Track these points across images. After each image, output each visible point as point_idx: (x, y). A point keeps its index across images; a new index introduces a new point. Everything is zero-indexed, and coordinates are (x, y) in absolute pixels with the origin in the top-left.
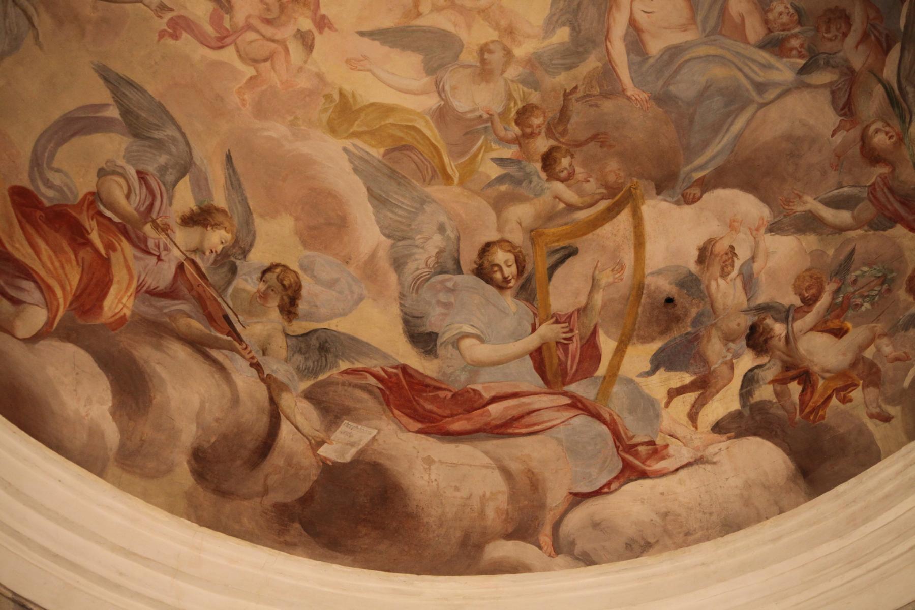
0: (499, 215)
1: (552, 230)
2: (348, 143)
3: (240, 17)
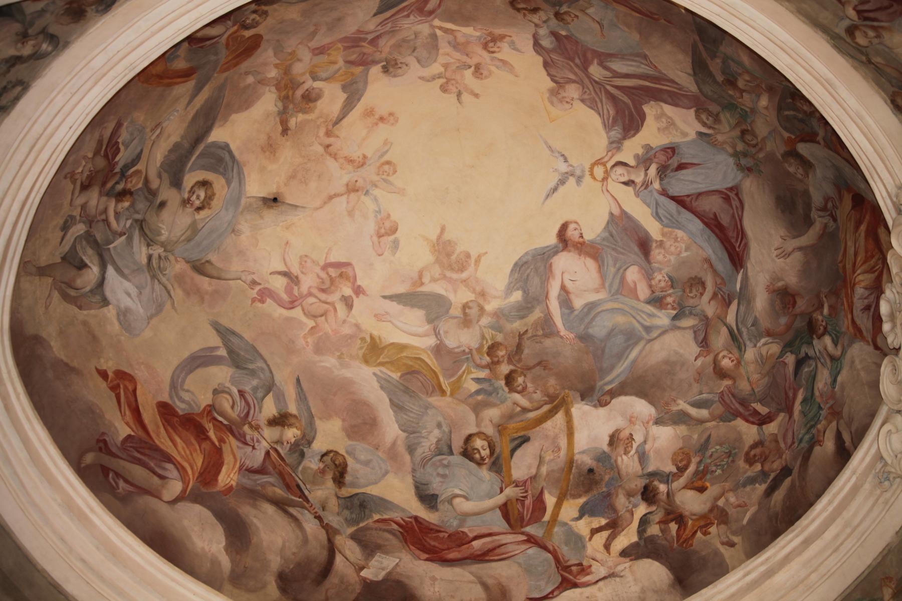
0: (477, 416)
1: (512, 425)
2: (376, 370)
3: (304, 288)
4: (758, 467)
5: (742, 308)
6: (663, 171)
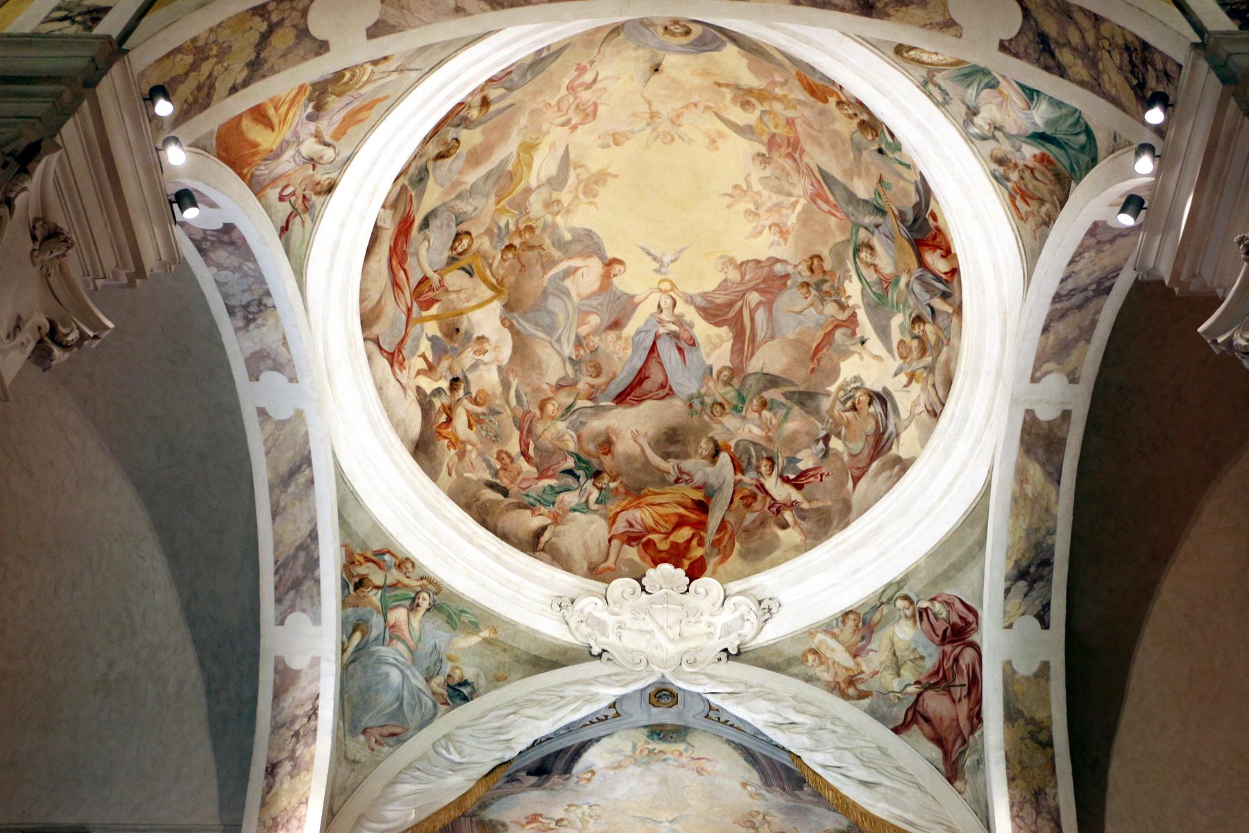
0: (483, 234)
1: (480, 262)
2: (515, 153)
6: (674, 336)
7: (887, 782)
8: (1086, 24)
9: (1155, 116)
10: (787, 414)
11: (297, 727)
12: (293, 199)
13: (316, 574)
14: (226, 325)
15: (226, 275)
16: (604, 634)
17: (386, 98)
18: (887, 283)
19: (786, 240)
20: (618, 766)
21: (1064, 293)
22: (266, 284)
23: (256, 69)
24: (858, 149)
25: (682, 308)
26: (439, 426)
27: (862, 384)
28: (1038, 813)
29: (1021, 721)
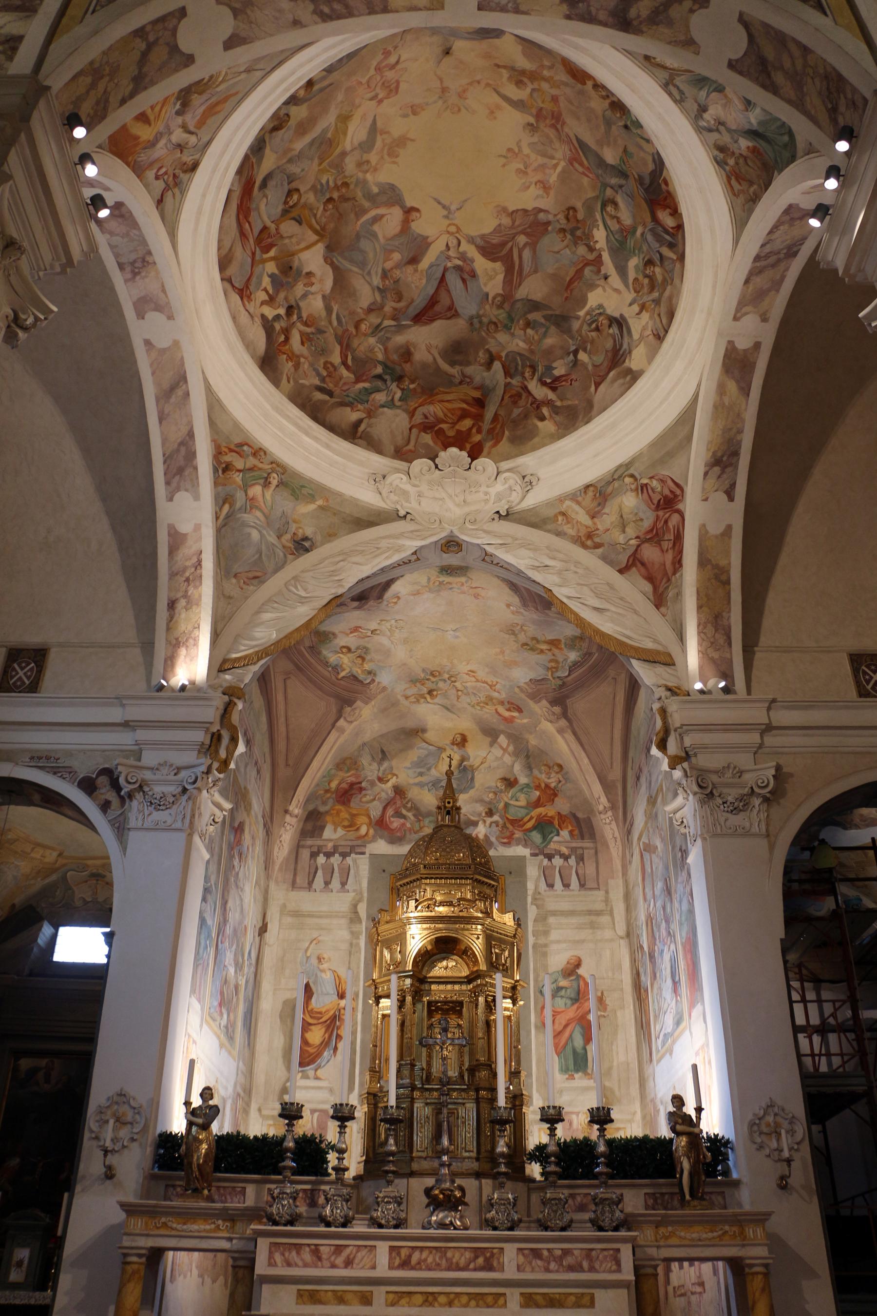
1: (307, 212)
2: (333, 123)
4: (325, 373)
5: (393, 329)
6: (458, 268)
7: (613, 608)
8: (796, 52)
9: (842, 146)
10: (546, 332)
11: (187, 574)
12: (166, 177)
13: (194, 463)
14: (118, 278)
15: (117, 240)
16: (408, 501)
17: (237, 93)
18: (626, 233)
19: (548, 194)
20: (418, 593)
21: (763, 255)
22: (147, 245)
23: (140, 83)
24: (608, 123)
25: (465, 247)
26: (279, 345)
27: (605, 311)
28: (716, 630)
29: (709, 567)
